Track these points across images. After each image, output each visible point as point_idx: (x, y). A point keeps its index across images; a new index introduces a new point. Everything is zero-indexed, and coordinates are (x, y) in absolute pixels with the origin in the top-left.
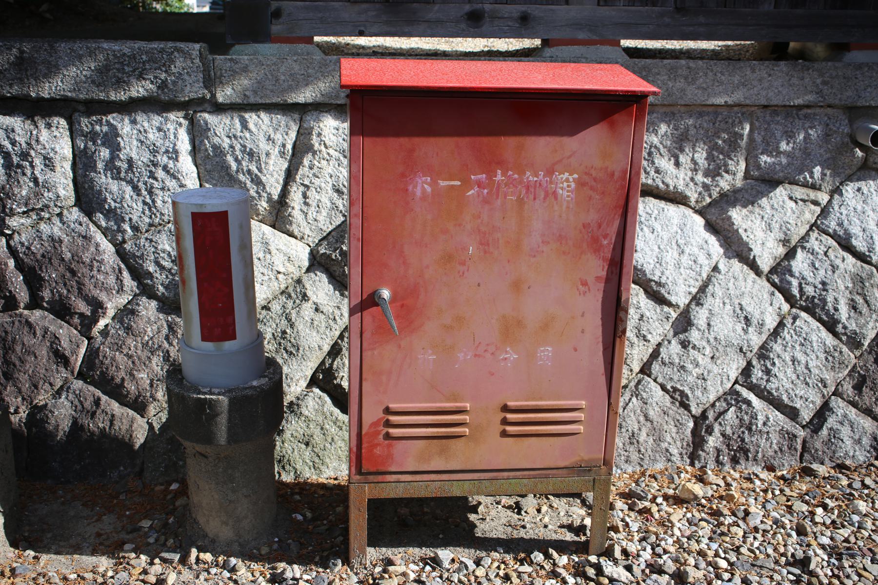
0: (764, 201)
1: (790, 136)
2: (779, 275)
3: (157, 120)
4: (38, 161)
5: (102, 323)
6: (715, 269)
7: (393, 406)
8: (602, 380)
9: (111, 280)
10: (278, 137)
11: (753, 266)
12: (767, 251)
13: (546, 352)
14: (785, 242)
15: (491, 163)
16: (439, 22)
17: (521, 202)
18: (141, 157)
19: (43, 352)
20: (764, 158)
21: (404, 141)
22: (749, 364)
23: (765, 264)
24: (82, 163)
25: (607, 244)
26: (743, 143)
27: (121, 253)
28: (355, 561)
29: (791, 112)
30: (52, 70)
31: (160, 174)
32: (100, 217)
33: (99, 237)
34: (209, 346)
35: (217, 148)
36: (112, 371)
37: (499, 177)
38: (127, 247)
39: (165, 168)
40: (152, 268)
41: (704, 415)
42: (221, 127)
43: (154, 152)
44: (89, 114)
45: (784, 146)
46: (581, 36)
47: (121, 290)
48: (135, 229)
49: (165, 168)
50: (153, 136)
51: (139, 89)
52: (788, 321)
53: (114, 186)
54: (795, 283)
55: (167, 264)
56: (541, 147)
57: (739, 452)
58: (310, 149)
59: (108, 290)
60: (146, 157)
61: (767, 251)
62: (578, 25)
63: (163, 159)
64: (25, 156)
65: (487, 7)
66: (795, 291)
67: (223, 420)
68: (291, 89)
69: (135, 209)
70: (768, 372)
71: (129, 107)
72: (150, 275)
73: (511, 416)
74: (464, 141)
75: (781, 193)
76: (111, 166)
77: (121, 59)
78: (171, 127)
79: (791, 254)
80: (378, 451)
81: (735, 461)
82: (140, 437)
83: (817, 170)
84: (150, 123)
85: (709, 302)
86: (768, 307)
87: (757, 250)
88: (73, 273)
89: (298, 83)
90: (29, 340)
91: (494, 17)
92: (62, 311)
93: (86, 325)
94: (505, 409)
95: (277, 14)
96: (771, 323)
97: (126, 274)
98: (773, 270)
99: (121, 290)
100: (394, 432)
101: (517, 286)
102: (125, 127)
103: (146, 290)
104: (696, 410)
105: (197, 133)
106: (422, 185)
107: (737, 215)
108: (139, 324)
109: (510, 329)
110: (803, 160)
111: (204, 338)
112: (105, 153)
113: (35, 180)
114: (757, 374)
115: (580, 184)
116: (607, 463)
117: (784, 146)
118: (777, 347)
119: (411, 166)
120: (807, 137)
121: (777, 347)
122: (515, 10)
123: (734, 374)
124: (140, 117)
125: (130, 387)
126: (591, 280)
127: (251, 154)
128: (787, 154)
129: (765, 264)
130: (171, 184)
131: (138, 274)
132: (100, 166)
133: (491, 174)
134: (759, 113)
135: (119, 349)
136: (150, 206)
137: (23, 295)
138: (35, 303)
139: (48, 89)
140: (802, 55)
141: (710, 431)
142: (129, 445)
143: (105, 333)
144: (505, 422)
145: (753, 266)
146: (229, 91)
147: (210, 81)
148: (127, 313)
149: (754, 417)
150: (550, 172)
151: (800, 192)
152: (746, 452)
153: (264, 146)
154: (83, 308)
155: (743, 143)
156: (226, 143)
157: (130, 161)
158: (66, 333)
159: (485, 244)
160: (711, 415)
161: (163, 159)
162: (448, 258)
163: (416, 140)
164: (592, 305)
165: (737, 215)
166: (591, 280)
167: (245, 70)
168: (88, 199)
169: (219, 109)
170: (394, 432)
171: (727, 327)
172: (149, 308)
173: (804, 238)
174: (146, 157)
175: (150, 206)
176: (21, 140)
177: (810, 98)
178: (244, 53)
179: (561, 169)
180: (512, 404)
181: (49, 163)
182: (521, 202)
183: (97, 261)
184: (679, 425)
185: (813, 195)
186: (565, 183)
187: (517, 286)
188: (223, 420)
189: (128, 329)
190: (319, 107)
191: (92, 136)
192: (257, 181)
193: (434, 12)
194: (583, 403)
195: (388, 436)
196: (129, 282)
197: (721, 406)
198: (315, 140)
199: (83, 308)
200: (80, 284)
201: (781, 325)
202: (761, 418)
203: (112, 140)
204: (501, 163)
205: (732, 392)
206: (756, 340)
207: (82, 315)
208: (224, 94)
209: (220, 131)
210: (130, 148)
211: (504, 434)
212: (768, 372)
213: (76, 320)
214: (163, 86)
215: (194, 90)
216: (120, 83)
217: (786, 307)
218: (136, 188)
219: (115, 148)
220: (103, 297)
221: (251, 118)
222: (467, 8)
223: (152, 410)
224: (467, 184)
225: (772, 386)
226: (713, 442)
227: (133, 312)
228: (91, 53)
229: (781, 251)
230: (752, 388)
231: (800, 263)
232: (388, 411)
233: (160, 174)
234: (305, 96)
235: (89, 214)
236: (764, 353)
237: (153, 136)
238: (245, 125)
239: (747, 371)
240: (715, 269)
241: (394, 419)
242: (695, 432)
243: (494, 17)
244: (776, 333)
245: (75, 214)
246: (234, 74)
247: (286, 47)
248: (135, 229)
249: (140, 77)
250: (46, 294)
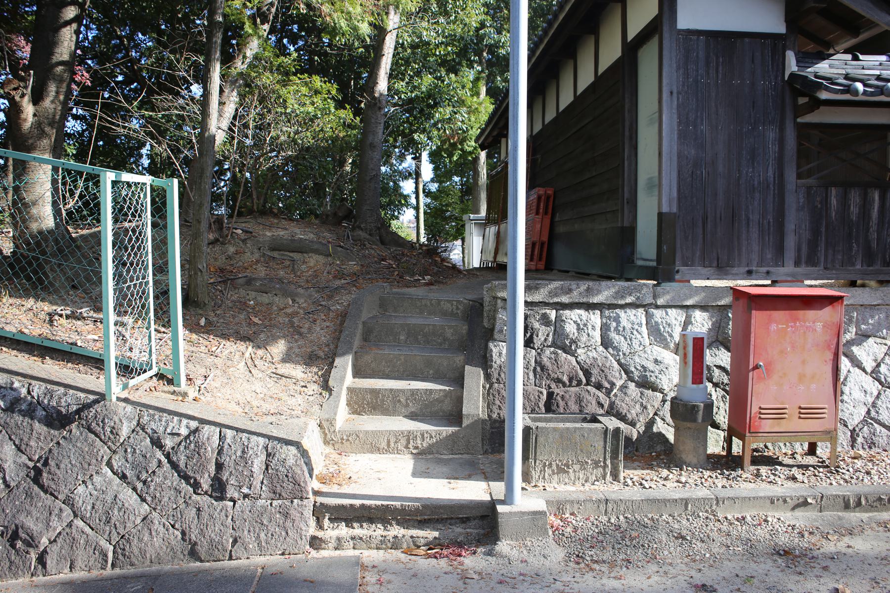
0: (865, 344)
1: (872, 317)
2: (875, 374)
3: (634, 311)
4: (590, 327)
5: (615, 391)
6: (849, 371)
7: (763, 406)
8: (833, 397)
9: (617, 374)
10: (679, 318)
11: (864, 370)
12: (869, 365)
13: (813, 386)
14: (875, 360)
15: (795, 319)
16: (737, 274)
17: (805, 332)
18: (628, 326)
19: (594, 402)
20: (863, 326)
21: (768, 312)
22: (869, 409)
23: (869, 370)
24: (605, 328)
25: (833, 347)
26: (854, 320)
27: (619, 362)
28: (745, 469)
29: (872, 306)
30: (599, 292)
31: (635, 332)
32: (610, 350)
33: (611, 358)
34: (695, 386)
35: (656, 322)
36: (621, 410)
37: (798, 324)
38: (623, 361)
39: (637, 330)
40: (633, 369)
41: (854, 429)
42: (658, 314)
43: (633, 324)
44: (609, 309)
45: (870, 321)
46: (789, 279)
47: (621, 378)
48: (624, 354)
49: (637, 330)
50: (633, 318)
51: (629, 300)
52: (882, 392)
53: (617, 337)
54: (882, 377)
55: (639, 368)
56: (811, 314)
57: (872, 445)
58: (691, 323)
59: (616, 378)
60: (630, 326)
61: (869, 365)
62: (788, 275)
63: (636, 327)
64: (585, 325)
65: (754, 268)
66: (883, 380)
67: (701, 413)
68: (685, 300)
69: (624, 347)
70: (877, 412)
71: (622, 307)
72: (632, 372)
73: (802, 411)
74: (787, 312)
75: (871, 340)
76: (616, 329)
77: (624, 289)
78: (639, 314)
79: (878, 365)
80: (756, 424)
81: (870, 448)
82: (635, 437)
83: (884, 331)
84: (631, 312)
85: (848, 384)
86: (874, 387)
87: (865, 364)
88: (603, 371)
89: (687, 299)
90: (589, 398)
91: (757, 272)
92: (599, 386)
93: (608, 393)
94: (800, 408)
95: (678, 272)
96: (875, 393)
97: (622, 372)
98: (872, 372)
99: (621, 378)
100: (763, 416)
101: (803, 362)
102: (621, 313)
103: (631, 379)
104: (851, 428)
105: (649, 316)
106: (774, 327)
107: (855, 349)
108: (629, 392)
109: (801, 378)
110: (878, 327)
111: (693, 383)
112: (614, 324)
113: (588, 335)
114: (873, 414)
115: (824, 326)
116: (836, 430)
117: (870, 321)
118: (879, 403)
119: (770, 320)
120: (879, 317)
121: (879, 403)
122: (764, 269)
123: (864, 414)
124: (628, 310)
125: (629, 416)
126: (828, 360)
127: (669, 325)
128: (872, 324)
129: (869, 370)
130: (639, 336)
131: (627, 372)
132: (612, 329)
133: (795, 323)
134: (859, 308)
135: (623, 401)
136: (630, 345)
137: (584, 380)
138: (588, 384)
139: (596, 300)
140: (863, 286)
141: (858, 435)
142: (631, 440)
143: (615, 395)
144: (800, 413)
145: (864, 370)
146: (662, 300)
147: (655, 297)
148: (624, 387)
149: (875, 430)
150: (814, 322)
151: (879, 340)
152: (874, 444)
153: (674, 322)
154: (607, 385)
155: (854, 320)
156: (660, 321)
157: (624, 328)
158: (601, 396)
159: (793, 347)
160: (857, 429)
161: (636, 327)
162: (782, 352)
163: (772, 312)
164: (828, 369)
165: (855, 349)
166: (828, 360)
167: (668, 292)
168: (606, 343)
169: (657, 307)
170: (763, 416)
171: (858, 395)
172: (632, 385)
173: (883, 359)
174: (630, 326)
175: (630, 345)
176: (584, 318)
177: (879, 302)
178: (667, 286)
179: (818, 321)
180: (802, 406)
181: (593, 328)
182: (805, 332)
183: (611, 368)
184: (844, 433)
185: (884, 341)
186: (819, 326)
187: (803, 362)
188: (701, 413)
189: (625, 394)
190: (694, 307)
191: (609, 318)
192: (671, 336)
193: (735, 270)
194: (826, 406)
195: (760, 418)
196: (624, 376)
197: (860, 426)
198: (693, 320)
199: (607, 385)
200: (606, 377)
201: (879, 394)
202: (878, 430)
203: (617, 319)
204: (798, 319)
205: (864, 420)
206: (870, 400)
207: (606, 388)
208: (660, 302)
209: (658, 316)
210: (624, 322)
211: (800, 418)
212: (877, 412)
213: (604, 390)
214: (638, 298)
215: (649, 300)
216: (623, 297)
217: (880, 387)
218: (625, 338)
219: (618, 323)
220: (615, 381)
221: (669, 310)
222: (747, 269)
223: (638, 426)
224: (788, 327)
225: (880, 418)
226: (860, 440)
227: (626, 387)
228: (614, 286)
229: (874, 364)
230: (872, 419)
231: (883, 369)
232: (760, 408)
233: (635, 332)
234: (689, 302)
235: (606, 349)
236: (874, 405)
237: (633, 318)
238: (667, 314)
239: (868, 412)
240: (849, 371)
241: (763, 411)
242: (851, 436)
243: (757, 272)
244: (878, 397)
245: (601, 349)
246: (664, 294)
247: (681, 284)
248: (624, 354)
249: (630, 295)
250: (593, 379)
